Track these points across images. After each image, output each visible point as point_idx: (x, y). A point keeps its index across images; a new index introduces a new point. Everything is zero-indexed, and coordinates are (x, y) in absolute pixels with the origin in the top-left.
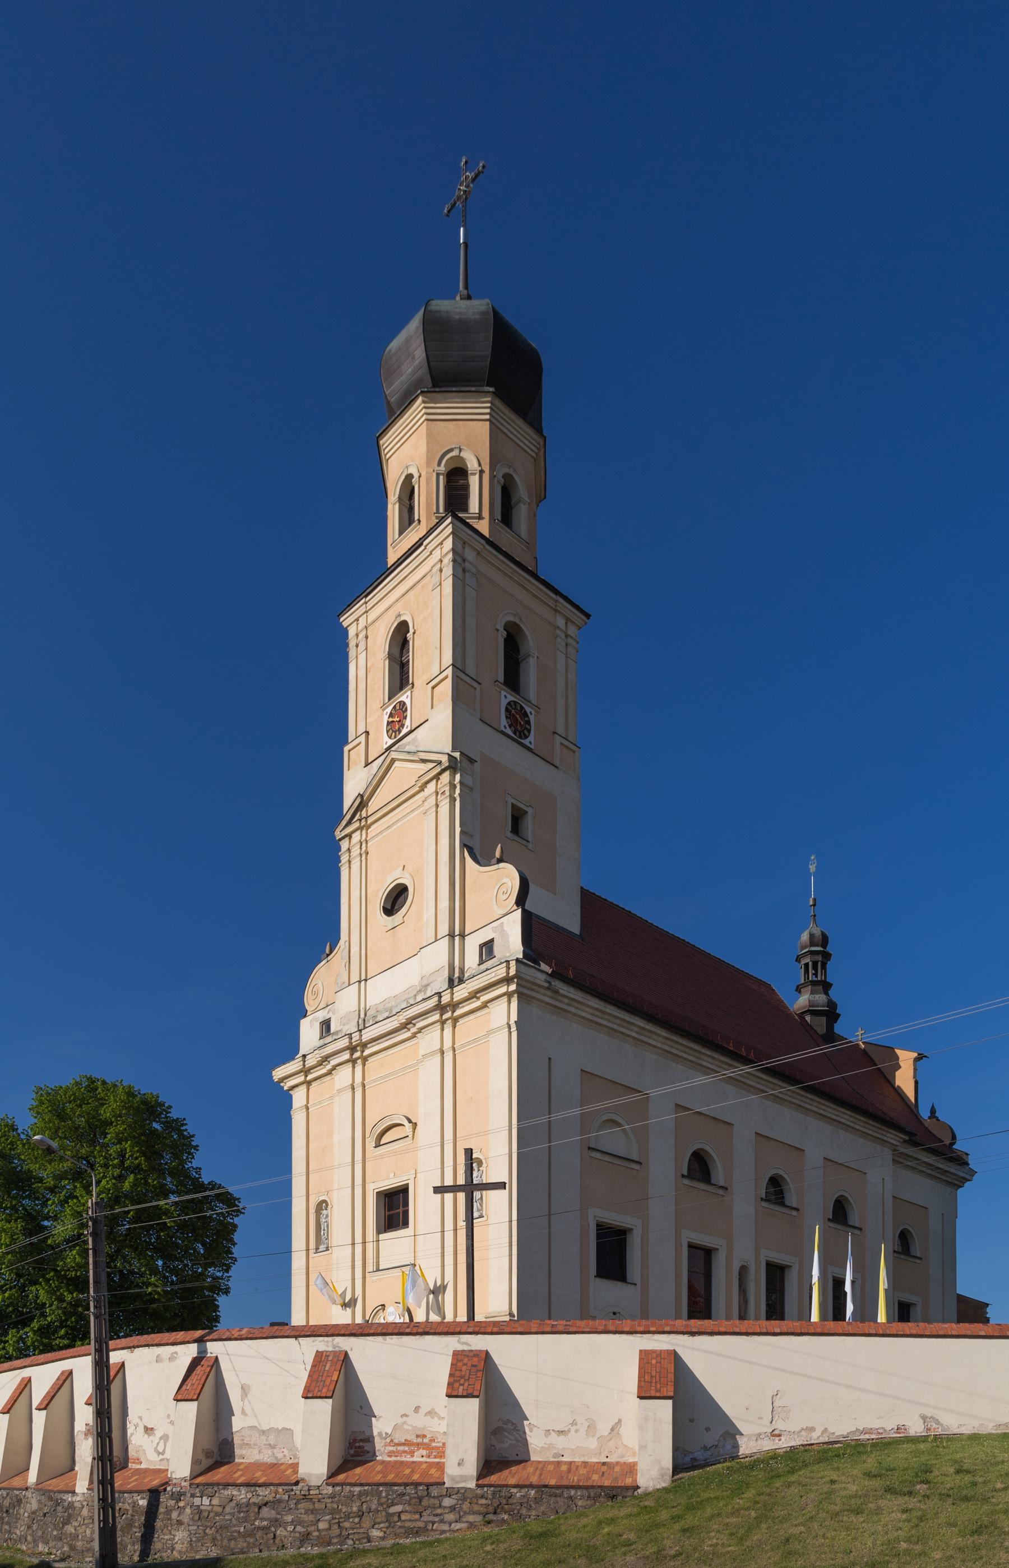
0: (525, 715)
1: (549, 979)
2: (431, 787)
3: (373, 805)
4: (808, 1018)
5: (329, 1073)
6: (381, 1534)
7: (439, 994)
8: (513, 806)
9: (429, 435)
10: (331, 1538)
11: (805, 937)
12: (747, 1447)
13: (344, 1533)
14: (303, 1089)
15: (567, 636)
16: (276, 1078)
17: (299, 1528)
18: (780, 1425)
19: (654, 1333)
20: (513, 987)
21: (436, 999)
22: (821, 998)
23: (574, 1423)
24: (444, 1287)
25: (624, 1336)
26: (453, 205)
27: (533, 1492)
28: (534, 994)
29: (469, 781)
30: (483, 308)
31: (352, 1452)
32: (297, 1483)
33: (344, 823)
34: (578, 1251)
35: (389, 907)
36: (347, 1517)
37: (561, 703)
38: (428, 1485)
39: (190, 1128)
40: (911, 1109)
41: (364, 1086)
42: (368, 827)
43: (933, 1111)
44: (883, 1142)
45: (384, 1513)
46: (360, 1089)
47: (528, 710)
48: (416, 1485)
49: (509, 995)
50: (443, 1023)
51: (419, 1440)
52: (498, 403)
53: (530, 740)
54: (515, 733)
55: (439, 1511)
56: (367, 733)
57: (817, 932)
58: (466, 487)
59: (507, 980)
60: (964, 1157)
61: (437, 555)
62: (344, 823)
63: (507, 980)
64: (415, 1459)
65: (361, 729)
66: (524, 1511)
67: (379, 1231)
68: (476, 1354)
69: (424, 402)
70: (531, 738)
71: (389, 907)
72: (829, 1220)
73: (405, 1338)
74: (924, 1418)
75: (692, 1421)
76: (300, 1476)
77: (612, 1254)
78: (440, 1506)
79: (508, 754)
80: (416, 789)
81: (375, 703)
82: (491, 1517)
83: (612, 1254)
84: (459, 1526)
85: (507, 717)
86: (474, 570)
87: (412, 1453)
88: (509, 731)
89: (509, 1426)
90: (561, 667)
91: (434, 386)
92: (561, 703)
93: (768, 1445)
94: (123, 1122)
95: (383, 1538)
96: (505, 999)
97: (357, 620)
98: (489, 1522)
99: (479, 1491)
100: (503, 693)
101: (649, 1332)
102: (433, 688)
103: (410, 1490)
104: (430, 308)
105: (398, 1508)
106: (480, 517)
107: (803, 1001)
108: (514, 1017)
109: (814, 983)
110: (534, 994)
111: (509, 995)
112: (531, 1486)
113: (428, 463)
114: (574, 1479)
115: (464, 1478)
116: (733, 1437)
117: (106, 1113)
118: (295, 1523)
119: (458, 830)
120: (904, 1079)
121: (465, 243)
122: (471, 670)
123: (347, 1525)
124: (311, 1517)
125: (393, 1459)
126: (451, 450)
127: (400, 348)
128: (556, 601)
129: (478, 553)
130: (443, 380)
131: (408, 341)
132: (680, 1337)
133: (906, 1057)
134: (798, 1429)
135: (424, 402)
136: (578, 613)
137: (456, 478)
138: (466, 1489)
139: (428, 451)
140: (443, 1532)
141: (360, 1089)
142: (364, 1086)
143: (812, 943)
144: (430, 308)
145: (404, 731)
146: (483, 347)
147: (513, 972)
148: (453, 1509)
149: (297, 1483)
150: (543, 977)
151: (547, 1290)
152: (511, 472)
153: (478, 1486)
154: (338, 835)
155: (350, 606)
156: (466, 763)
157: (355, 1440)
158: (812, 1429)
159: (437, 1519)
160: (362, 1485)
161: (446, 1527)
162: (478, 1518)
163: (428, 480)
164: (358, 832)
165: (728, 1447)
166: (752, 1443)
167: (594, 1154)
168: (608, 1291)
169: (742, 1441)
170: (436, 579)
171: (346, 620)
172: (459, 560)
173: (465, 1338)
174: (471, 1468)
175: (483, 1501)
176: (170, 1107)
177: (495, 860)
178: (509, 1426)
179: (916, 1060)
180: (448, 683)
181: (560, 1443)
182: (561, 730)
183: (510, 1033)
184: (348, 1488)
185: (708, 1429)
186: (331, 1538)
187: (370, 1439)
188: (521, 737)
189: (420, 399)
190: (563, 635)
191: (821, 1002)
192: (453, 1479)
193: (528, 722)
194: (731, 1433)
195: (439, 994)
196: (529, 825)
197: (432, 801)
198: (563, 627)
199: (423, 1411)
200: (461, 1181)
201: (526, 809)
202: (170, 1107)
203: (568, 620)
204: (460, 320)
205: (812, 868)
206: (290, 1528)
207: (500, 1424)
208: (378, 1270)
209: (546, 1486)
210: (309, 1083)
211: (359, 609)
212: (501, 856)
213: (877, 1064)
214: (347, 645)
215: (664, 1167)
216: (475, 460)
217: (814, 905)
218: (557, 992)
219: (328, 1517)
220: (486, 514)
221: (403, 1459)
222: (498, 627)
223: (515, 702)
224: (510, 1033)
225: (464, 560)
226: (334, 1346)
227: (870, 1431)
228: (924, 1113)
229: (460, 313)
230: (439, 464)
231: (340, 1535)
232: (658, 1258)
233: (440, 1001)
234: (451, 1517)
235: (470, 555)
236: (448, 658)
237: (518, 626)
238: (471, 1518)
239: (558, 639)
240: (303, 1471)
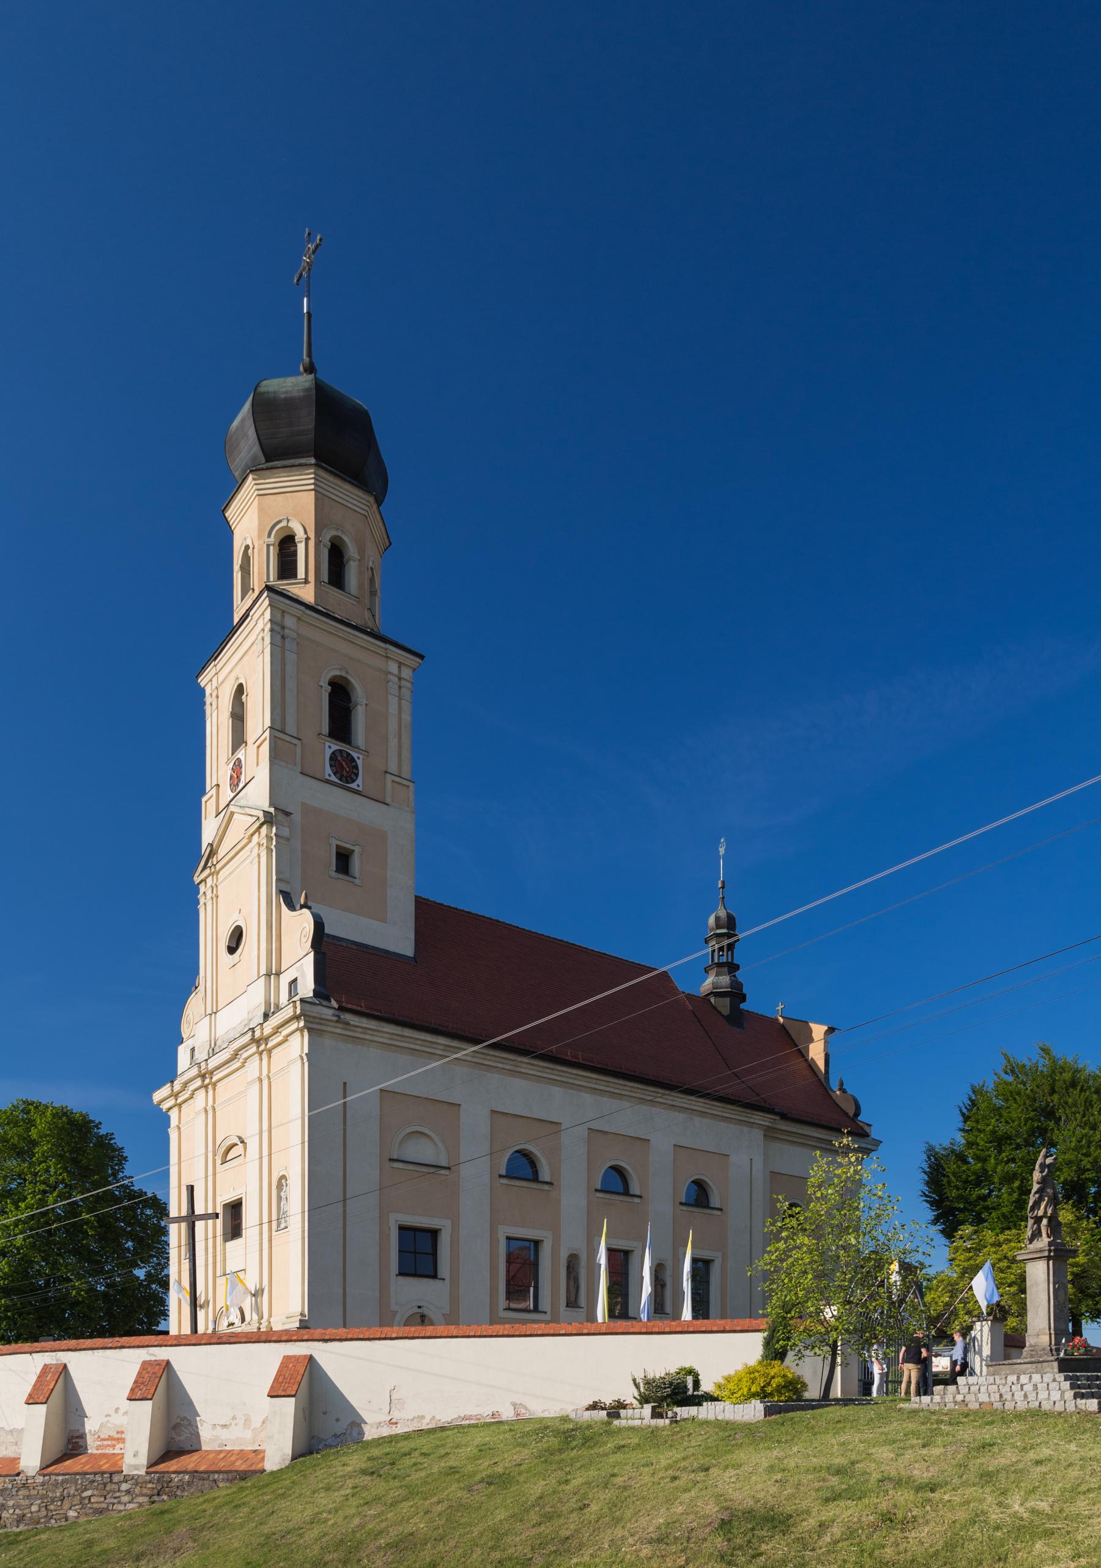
0: (353, 760)
1: (337, 1013)
2: (255, 838)
3: (222, 852)
4: (712, 1000)
5: (191, 1097)
6: (76, 1514)
7: (253, 1030)
8: (337, 846)
9: (261, 509)
10: (40, 1518)
11: (712, 920)
12: (370, 1433)
13: (50, 1514)
14: (176, 1109)
15: (400, 679)
16: (155, 1101)
17: (18, 1511)
18: (396, 1415)
19: (295, 1341)
20: (302, 1024)
21: (250, 1033)
22: (725, 980)
23: (234, 1418)
24: (263, 1290)
25: (272, 1344)
26: (301, 275)
27: (187, 1477)
28: (324, 1028)
29: (286, 832)
30: (307, 385)
31: (70, 1447)
32: (18, 1474)
33: (200, 869)
34: (374, 1247)
35: (234, 946)
36: (53, 1501)
37: (393, 743)
38: (111, 1474)
39: (119, 1142)
40: (819, 1082)
41: (214, 1109)
42: (218, 873)
44: (752, 1125)
46: (211, 1112)
47: (355, 755)
48: (103, 1473)
49: (301, 1030)
50: (261, 1054)
51: (119, 1436)
52: (321, 473)
53: (358, 784)
54: (340, 779)
55: (118, 1494)
56: (218, 785)
57: (722, 913)
58: (295, 553)
59: (296, 1018)
60: (866, 1128)
61: (260, 625)
62: (200, 869)
63: (296, 1018)
64: (116, 1451)
65: (214, 783)
66: (179, 1493)
67: (226, 1240)
68: (158, 1363)
69: (254, 479)
70: (359, 781)
71: (234, 946)
73: (108, 1351)
74: (514, 1405)
75: (325, 1413)
76: (21, 1468)
77: (419, 1252)
78: (119, 1491)
79: (335, 801)
80: (245, 841)
81: (223, 758)
82: (156, 1498)
83: (419, 1252)
84: (131, 1506)
85: (331, 766)
86: (295, 635)
87: (114, 1446)
88: (333, 778)
89: (185, 1422)
90: (393, 709)
91: (267, 461)
92: (393, 743)
93: (386, 1432)
94: (48, 1142)
95: (77, 1517)
96: (298, 1033)
97: (211, 680)
98: (153, 1502)
99: (148, 1478)
100: (327, 744)
101: (291, 1341)
102: (258, 747)
103: (98, 1478)
104: (261, 389)
105: (88, 1493)
106: (306, 581)
107: (708, 983)
108: (306, 1050)
109: (720, 965)
110: (324, 1028)
111: (301, 1030)
112: (185, 1472)
113: (260, 537)
114: (222, 1465)
115: (136, 1467)
116: (359, 1425)
117: (34, 1133)
118: (14, 1507)
119: (274, 878)
120: (816, 1052)
121: (308, 313)
122: (291, 728)
123: (52, 1507)
124: (27, 1502)
125: (100, 1451)
126: (280, 522)
127: (237, 428)
129: (299, 619)
130: (276, 454)
131: (243, 421)
132: (316, 1343)
133: (818, 1031)
134: (411, 1417)
135: (254, 479)
136: (411, 657)
137: (286, 545)
138: (139, 1476)
139: (259, 525)
140: (120, 1511)
141: (211, 1112)
142: (214, 1109)
143: (718, 926)
144: (261, 389)
145: (241, 785)
146: (307, 421)
147: (298, 1011)
148: (128, 1492)
149: (18, 1474)
150: (330, 1012)
151: (341, 1291)
152: (339, 534)
153: (147, 1473)
154: (197, 880)
155: (204, 668)
156: (281, 817)
157: (72, 1437)
158: (423, 1417)
160: (63, 1474)
161: (121, 1507)
162: (146, 1499)
163: (260, 551)
164: (210, 878)
165: (355, 1434)
166: (374, 1430)
168: (416, 1290)
169: (366, 1428)
170: (260, 647)
171: (203, 681)
172: (278, 629)
174: (143, 1460)
175: (150, 1485)
176: (100, 1123)
177: (298, 907)
178: (185, 1422)
179: (827, 1033)
180: (267, 743)
181: (224, 1435)
182: (393, 767)
183: (303, 1064)
184: (53, 1477)
185: (338, 1420)
186: (40, 1518)
187: (83, 1436)
189: (251, 477)
190: (396, 680)
191: (724, 984)
192: (130, 1466)
193: (356, 767)
194: (357, 1423)
195: (253, 1030)
196: (356, 864)
197: (256, 851)
198: (396, 672)
199: (121, 1411)
200: (184, 1213)
201: (352, 848)
202: (100, 1123)
203: (400, 664)
204: (285, 399)
205: (722, 851)
206: (11, 1511)
207: (178, 1420)
208: (225, 1275)
209: (196, 1472)
210: (180, 1105)
211: (210, 671)
212: (306, 903)
213: (789, 1039)
214: (204, 704)
215: (477, 1174)
216: (303, 524)
217: (723, 887)
218: (348, 1024)
219: (39, 1502)
220: (312, 578)
221: (107, 1451)
222: (321, 684)
223: (340, 751)
224: (303, 1064)
225: (283, 628)
227: (470, 1418)
228: (834, 1085)
229: (286, 392)
230: (269, 536)
231: (46, 1516)
232: (473, 1253)
233: (253, 1035)
234: (125, 1499)
235: (290, 622)
236: (268, 723)
237: (345, 678)
238: (140, 1499)
239: (390, 684)
240: (23, 1464)
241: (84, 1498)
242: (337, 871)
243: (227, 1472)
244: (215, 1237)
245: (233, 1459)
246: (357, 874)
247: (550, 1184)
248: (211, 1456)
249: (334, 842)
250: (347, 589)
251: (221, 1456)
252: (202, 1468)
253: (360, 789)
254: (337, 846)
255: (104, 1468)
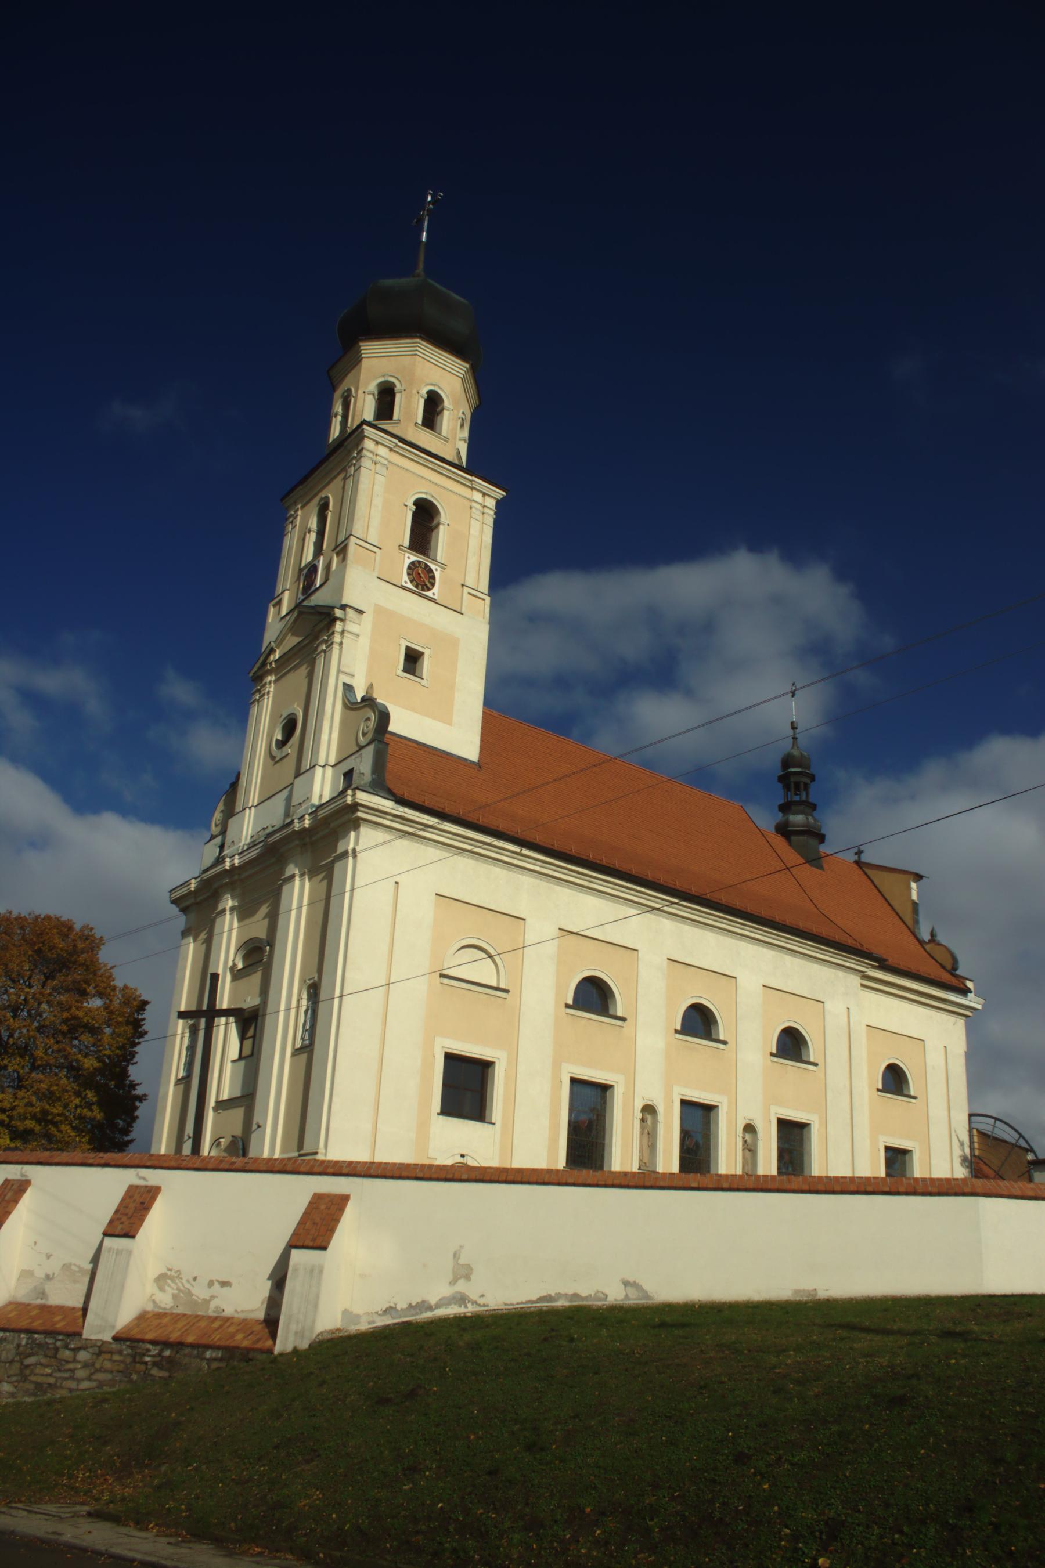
0: (430, 571)
8: (407, 648)
43: (933, 935)
45: (17, 1365)
47: (433, 567)
53: (435, 592)
54: (416, 587)
55: (71, 1366)
70: (435, 590)
72: (772, 1054)
78: (75, 1361)
85: (408, 574)
88: (410, 585)
114: (216, 1338)
128: (471, 481)
148: (86, 1365)
159: (66, 1375)
167: (446, 981)
173: (143, 1172)
175: (116, 1357)
188: (423, 590)
193: (433, 578)
196: (427, 665)
203: (484, 494)
211: (390, 347)
226: (22, 1175)
239: (474, 510)
241: (27, 1366)
242: (405, 670)
243: (219, 1348)
244: (288, 1009)
245: (232, 1330)
246: (424, 676)
247: (623, 1019)
248: (203, 1324)
249: (404, 644)
250: (438, 430)
251: (216, 1324)
252: (190, 1339)
253: (435, 597)
254: (407, 648)
255: (59, 1326)
